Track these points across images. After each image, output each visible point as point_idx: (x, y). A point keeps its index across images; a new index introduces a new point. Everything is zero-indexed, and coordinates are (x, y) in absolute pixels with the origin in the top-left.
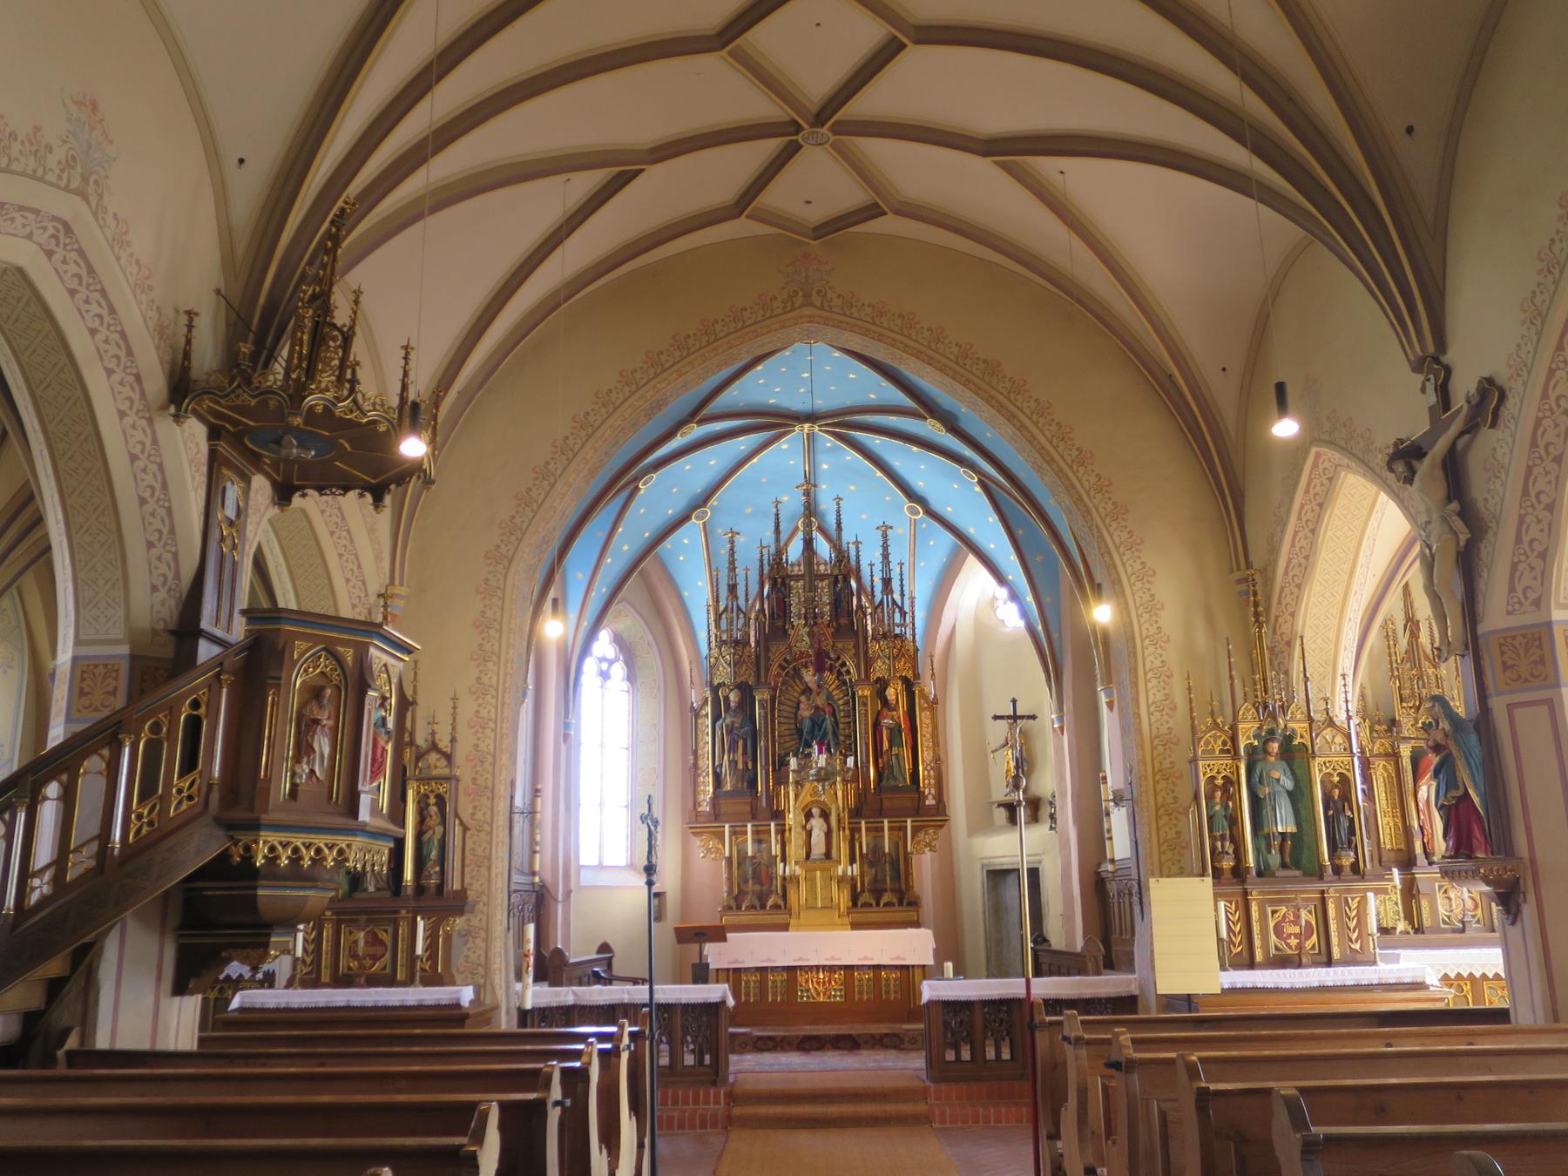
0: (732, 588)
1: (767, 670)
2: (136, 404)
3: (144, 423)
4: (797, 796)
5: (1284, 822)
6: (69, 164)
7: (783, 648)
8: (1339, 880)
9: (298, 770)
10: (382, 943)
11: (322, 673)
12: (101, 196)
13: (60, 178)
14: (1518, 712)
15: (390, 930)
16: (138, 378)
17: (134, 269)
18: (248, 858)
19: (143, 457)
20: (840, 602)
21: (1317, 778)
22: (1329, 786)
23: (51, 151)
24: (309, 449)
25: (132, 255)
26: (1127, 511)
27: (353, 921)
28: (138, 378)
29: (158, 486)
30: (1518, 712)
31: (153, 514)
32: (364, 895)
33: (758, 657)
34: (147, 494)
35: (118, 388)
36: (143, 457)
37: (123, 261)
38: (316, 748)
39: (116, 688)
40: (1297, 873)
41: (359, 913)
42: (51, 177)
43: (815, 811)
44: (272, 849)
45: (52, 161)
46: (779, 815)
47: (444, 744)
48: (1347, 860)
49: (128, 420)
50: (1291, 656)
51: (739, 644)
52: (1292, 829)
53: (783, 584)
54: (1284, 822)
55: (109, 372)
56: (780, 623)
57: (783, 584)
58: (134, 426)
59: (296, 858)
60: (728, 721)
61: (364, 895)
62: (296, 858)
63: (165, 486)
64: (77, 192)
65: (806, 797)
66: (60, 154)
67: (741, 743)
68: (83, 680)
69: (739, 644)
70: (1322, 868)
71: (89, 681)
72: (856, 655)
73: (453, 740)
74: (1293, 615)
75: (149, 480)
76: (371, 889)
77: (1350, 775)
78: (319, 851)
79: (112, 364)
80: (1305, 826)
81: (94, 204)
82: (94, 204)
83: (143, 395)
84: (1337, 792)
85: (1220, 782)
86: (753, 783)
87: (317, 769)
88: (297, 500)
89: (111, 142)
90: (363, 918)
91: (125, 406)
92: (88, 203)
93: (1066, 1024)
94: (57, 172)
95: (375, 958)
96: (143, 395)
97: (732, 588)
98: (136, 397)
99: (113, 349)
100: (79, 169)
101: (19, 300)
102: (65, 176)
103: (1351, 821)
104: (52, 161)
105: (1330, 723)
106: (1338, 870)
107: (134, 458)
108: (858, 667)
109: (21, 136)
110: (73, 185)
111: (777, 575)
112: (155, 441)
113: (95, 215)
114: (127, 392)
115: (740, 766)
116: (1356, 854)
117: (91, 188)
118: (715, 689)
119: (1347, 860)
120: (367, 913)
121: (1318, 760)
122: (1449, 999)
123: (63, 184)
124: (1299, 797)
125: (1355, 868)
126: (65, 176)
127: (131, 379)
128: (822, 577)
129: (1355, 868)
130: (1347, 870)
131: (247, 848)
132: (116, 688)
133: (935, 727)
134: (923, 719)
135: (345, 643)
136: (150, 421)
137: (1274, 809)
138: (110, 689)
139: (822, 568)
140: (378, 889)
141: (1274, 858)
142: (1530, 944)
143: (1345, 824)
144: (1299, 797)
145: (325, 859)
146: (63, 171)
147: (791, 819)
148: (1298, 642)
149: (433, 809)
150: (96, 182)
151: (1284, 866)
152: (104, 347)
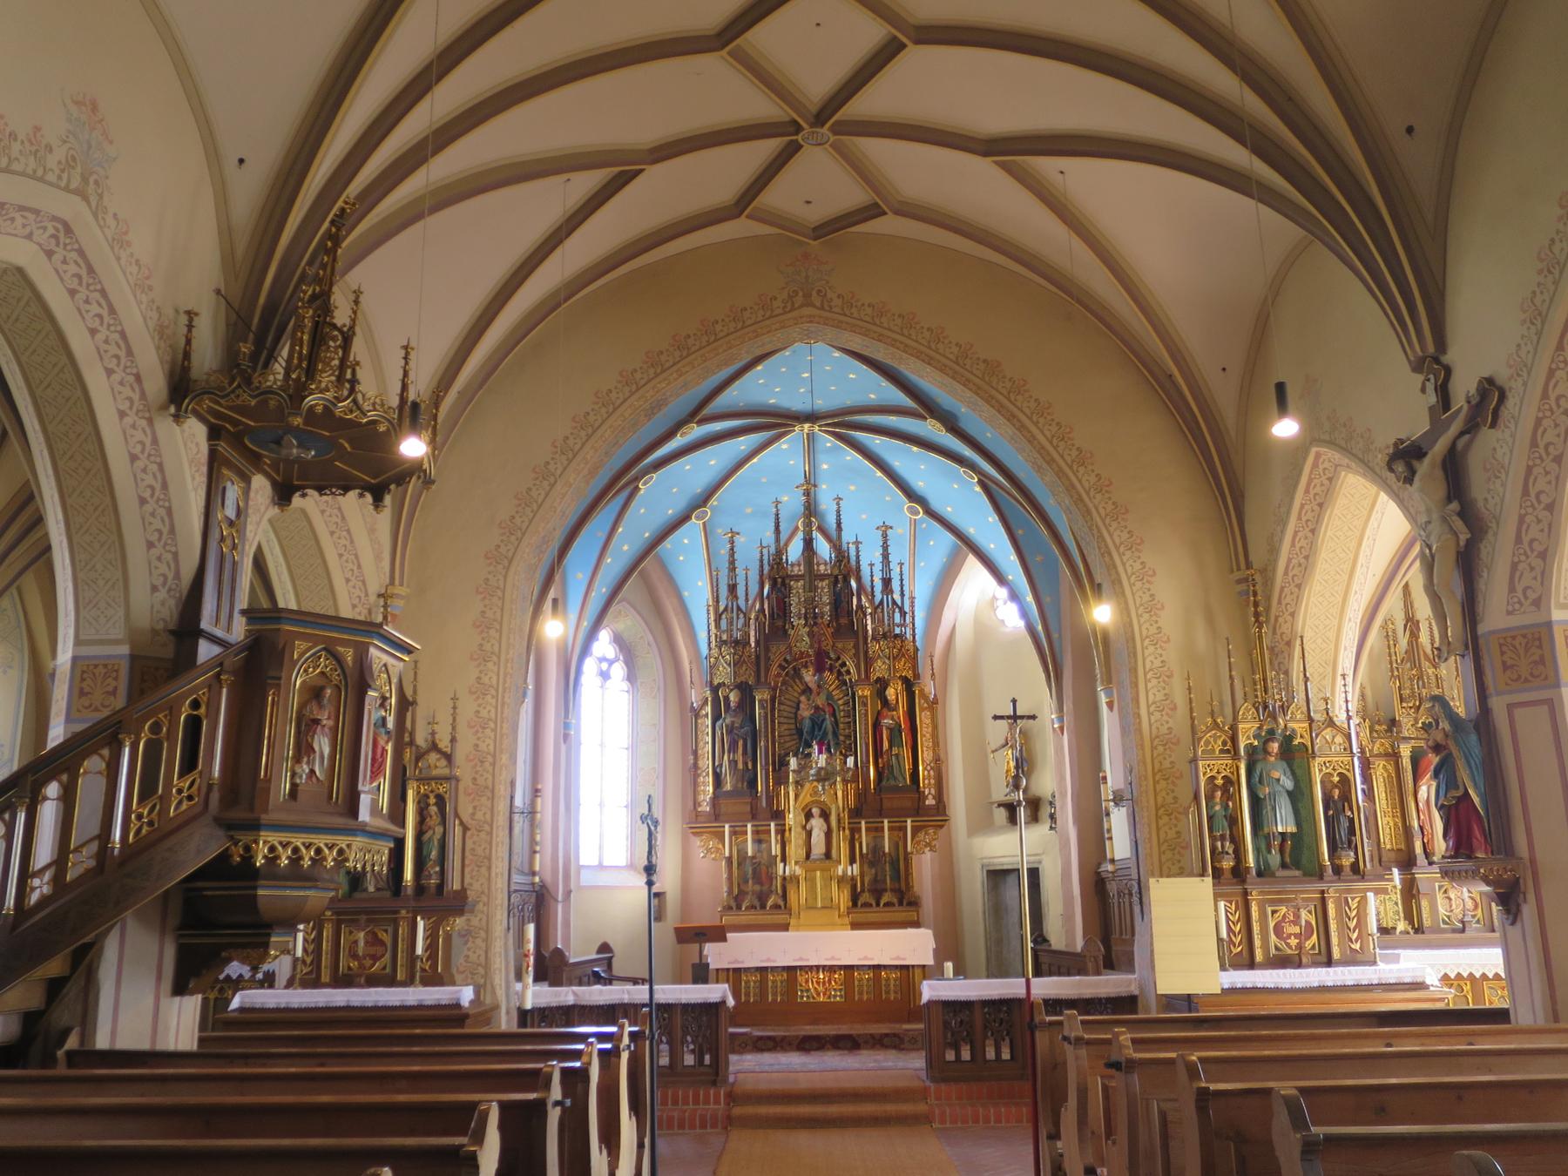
0: (732, 588)
1: (767, 670)
2: (136, 404)
3: (144, 423)
4: (797, 796)
5: (1284, 822)
6: (69, 164)
7: (783, 648)
8: (1339, 880)
9: (298, 770)
10: (382, 943)
11: (322, 673)
12: (101, 196)
13: (60, 178)
14: (1518, 712)
15: (390, 930)
16: (138, 378)
17: (134, 269)
18: (248, 858)
19: (143, 457)
20: (840, 602)
21: (1317, 778)
22: (1329, 786)
23: (51, 151)
24: (309, 449)
25: (132, 255)
26: (1127, 511)
27: (353, 921)
28: (138, 378)
29: (158, 486)
30: (1518, 712)
31: (153, 514)
32: (364, 895)
33: (758, 657)
34: (147, 494)
35: (118, 388)
36: (143, 457)
37: (123, 261)
38: (316, 748)
39: (116, 688)
40: (1297, 873)
41: (359, 913)
42: (51, 177)
43: (815, 811)
44: (272, 849)
45: (52, 161)
46: (779, 815)
47: (444, 744)
48: (1347, 860)
49: (128, 420)
50: (1291, 656)
51: (739, 644)
52: (1292, 829)
53: (783, 584)
54: (1284, 822)
55: (109, 372)
56: (780, 623)
57: (783, 584)
58: (134, 426)
59: (296, 858)
60: (728, 721)
61: (364, 895)
62: (296, 858)
63: (165, 486)
64: (77, 192)
65: (806, 797)
66: (60, 154)
67: (741, 743)
68: (83, 680)
69: (739, 644)
70: (1322, 868)
71: (89, 681)
72: (856, 655)
73: (453, 740)
74: (1293, 615)
75: (149, 480)
76: (371, 889)
77: (1350, 775)
78: (319, 851)
79: (112, 364)
80: (1305, 826)
81: (94, 204)
82: (94, 204)
83: (143, 395)
84: (1337, 792)
85: (1220, 782)
86: (753, 783)
87: (317, 769)
88: (297, 500)
89: (111, 142)
90: (363, 918)
91: (125, 406)
92: (88, 203)
93: (1066, 1024)
94: (57, 172)
95: (375, 958)
96: (143, 395)
97: (732, 588)
98: (136, 397)
99: (113, 349)
100: (79, 169)
101: (19, 300)
102: (65, 176)
103: (1351, 821)
104: (52, 161)
105: (1330, 723)
106: (1338, 870)
107: (134, 458)
108: (858, 667)
109: (21, 136)
110: (73, 185)
111: (777, 575)
112: (155, 441)
113: (95, 215)
114: (127, 392)
115: (740, 766)
116: (1356, 854)
117: (91, 188)
118: (715, 689)
119: (1347, 860)
120: (367, 913)
121: (1318, 760)
122: (1449, 999)
123: (63, 184)
124: (1299, 797)
125: (1355, 868)
126: (65, 176)
127: (131, 379)
128: (822, 577)
129: (1355, 868)
130: (1347, 870)
131: (247, 848)
132: (116, 688)
133: (935, 727)
134: (923, 719)
135: (345, 643)
136: (150, 421)
137: (1274, 809)
138: (110, 689)
139: (822, 568)
140: (378, 889)
141: (1274, 858)
143: (1345, 824)
144: (1299, 797)
145: (325, 859)
146: (63, 171)
147: (791, 819)
148: (1298, 642)
149: (433, 809)
150: (96, 182)
151: (1284, 866)
152: (104, 347)
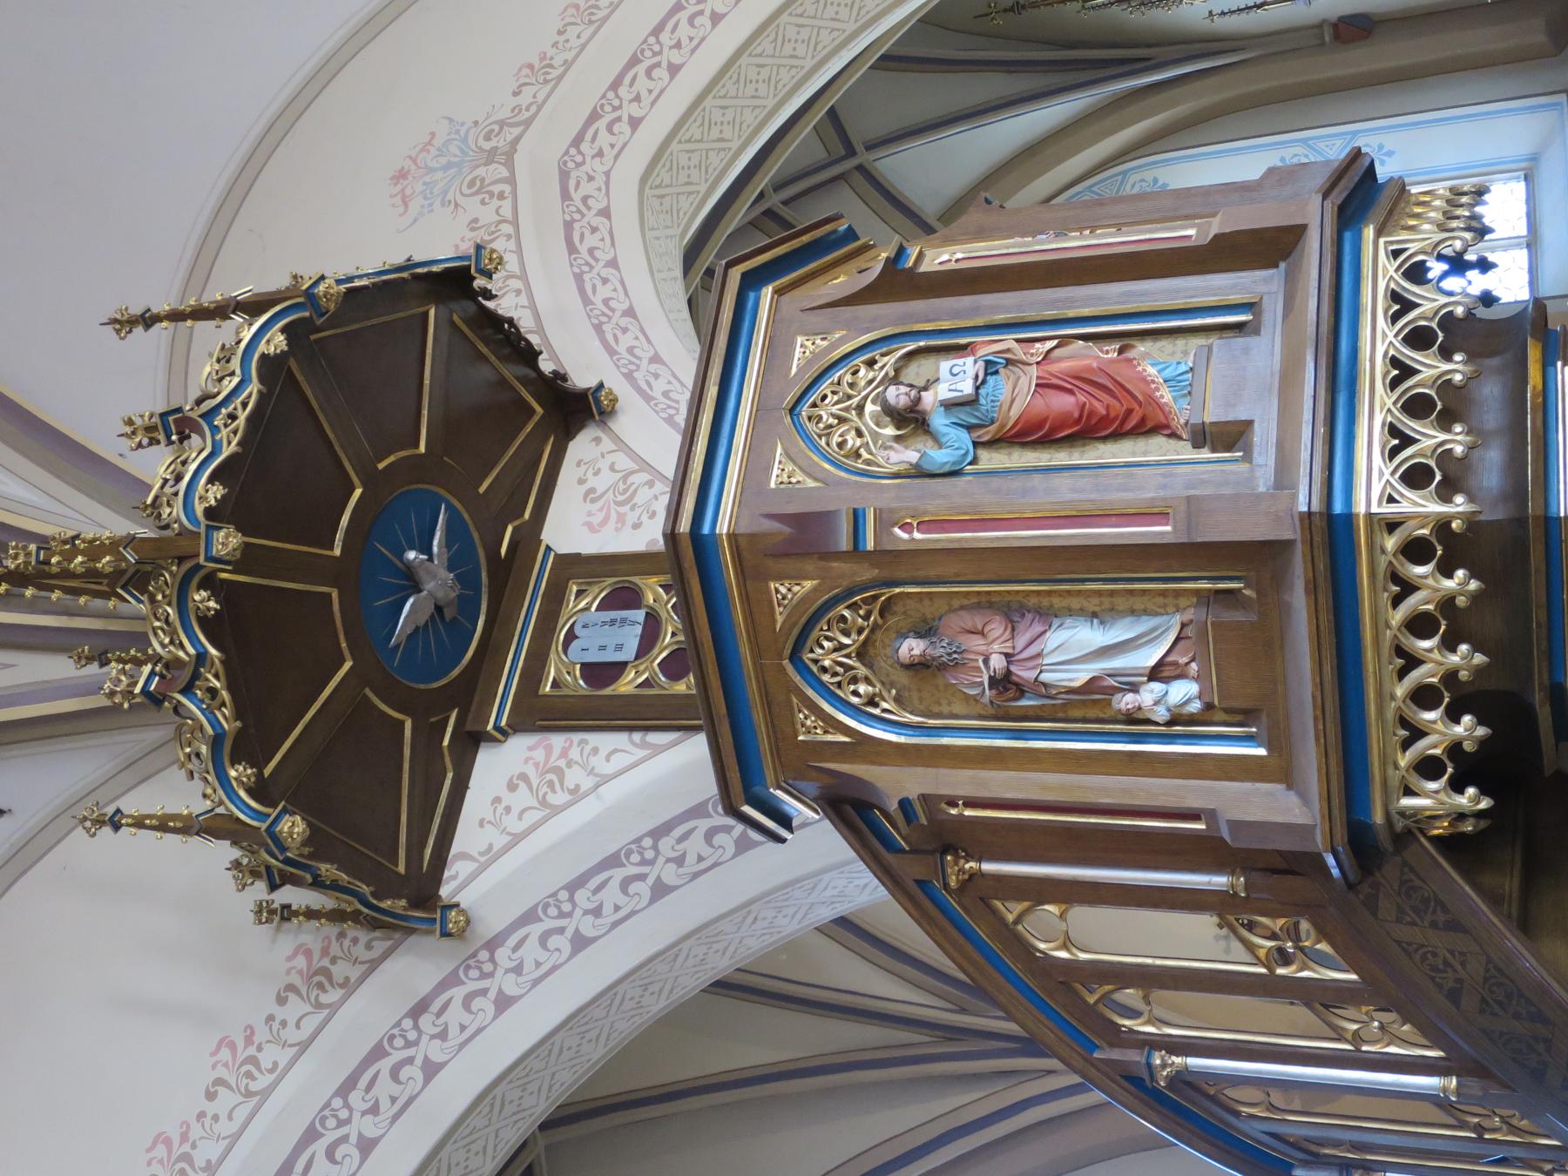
2: (472, 986)
3: (502, 954)
6: (479, 188)
9: (1161, 714)
11: (861, 654)
12: (502, 124)
13: (501, 196)
16: (417, 1011)
17: (572, 32)
18: (1444, 546)
19: (571, 926)
23: (476, 220)
24: (409, 566)
25: (555, 45)
28: (417, 1011)
29: (618, 874)
31: (680, 861)
34: (642, 889)
35: (455, 1037)
36: (571, 926)
37: (569, 56)
38: (1079, 676)
42: (507, 212)
44: (1428, 768)
49: (510, 986)
55: (431, 1070)
58: (518, 970)
59: (1449, 622)
62: (1449, 622)
63: (613, 861)
64: (509, 164)
66: (473, 207)
75: (612, 895)
78: (1420, 625)
79: (413, 1072)
81: (517, 131)
82: (517, 131)
83: (443, 986)
87: (1150, 657)
89: (433, 135)
91: (485, 1005)
92: (518, 139)
93: (879, 505)
96: (443, 986)
98: (458, 993)
99: (385, 1087)
100: (481, 171)
101: (662, 197)
102: (496, 189)
104: (487, 215)
107: (580, 943)
110: (505, 173)
112: (529, 917)
113: (528, 123)
114: (455, 1015)
117: (499, 142)
123: (507, 188)
126: (496, 189)
127: (426, 1021)
131: (1416, 550)
135: (758, 606)
136: (492, 945)
142: (1322, 600)
145: (1447, 604)
146: (491, 195)
150: (488, 138)
152: (387, 1110)
